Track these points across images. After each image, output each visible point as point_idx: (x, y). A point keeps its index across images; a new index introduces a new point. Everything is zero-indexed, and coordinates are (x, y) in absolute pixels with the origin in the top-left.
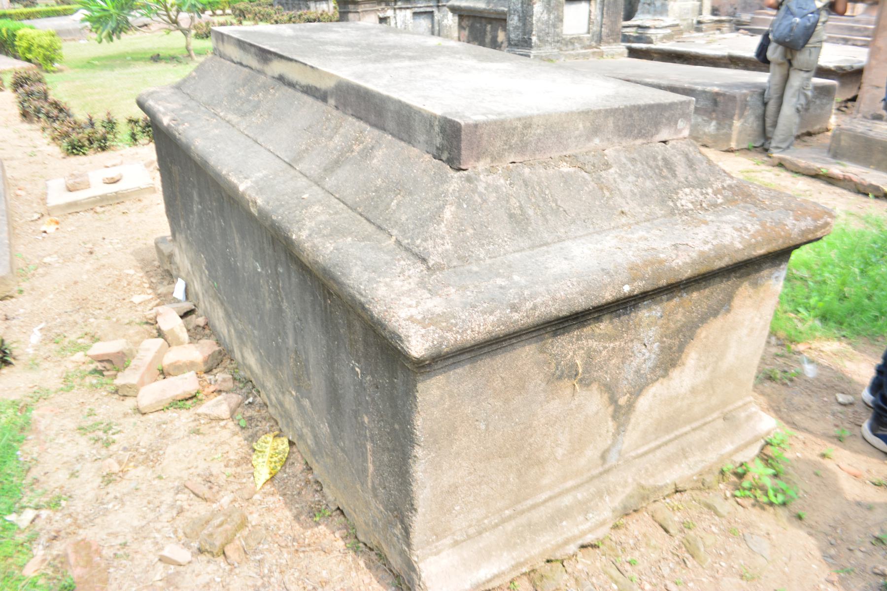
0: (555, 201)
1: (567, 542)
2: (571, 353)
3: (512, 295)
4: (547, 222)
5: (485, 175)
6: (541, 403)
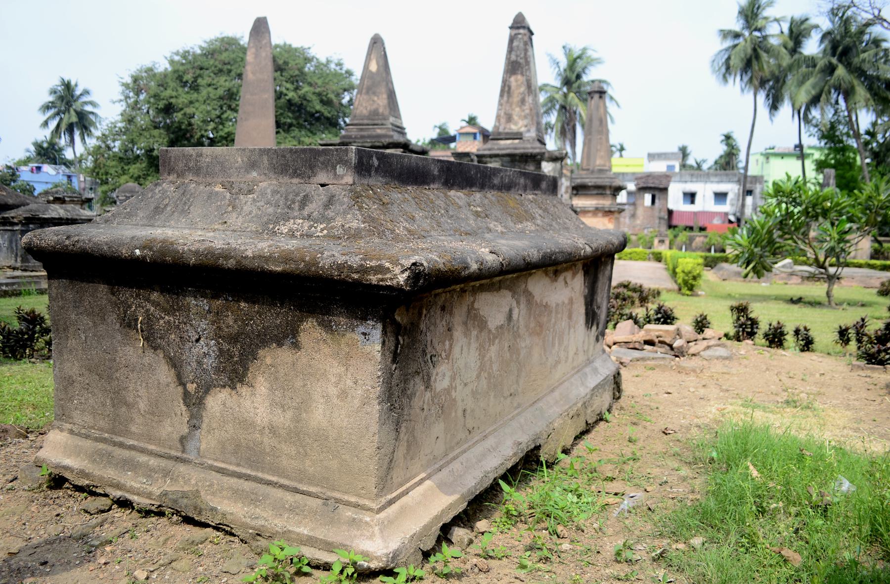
1: (118, 486)
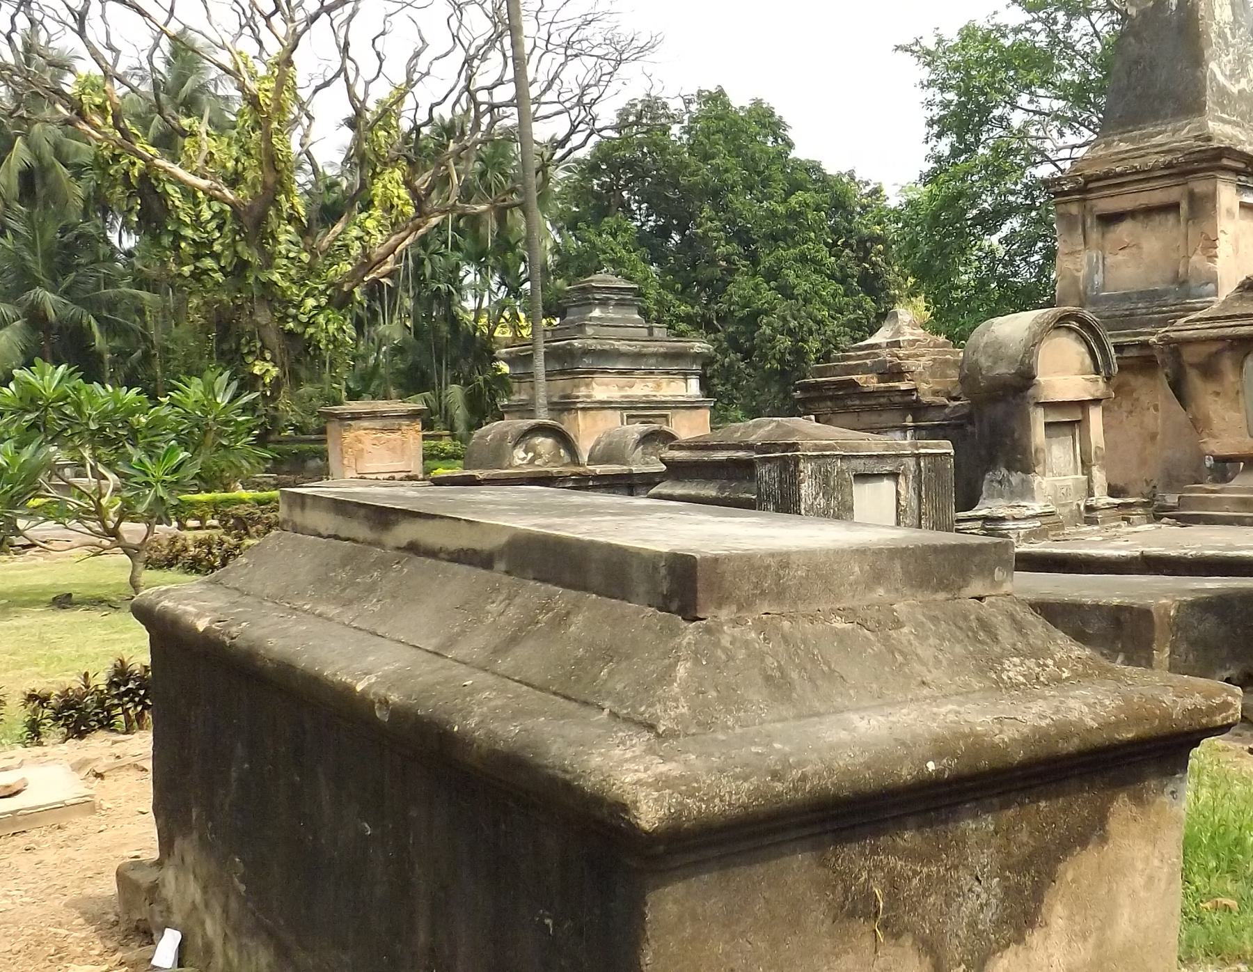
0: (828, 664)
2: (865, 875)
3: (772, 760)
4: (817, 689)
5: (731, 628)
6: (826, 955)
